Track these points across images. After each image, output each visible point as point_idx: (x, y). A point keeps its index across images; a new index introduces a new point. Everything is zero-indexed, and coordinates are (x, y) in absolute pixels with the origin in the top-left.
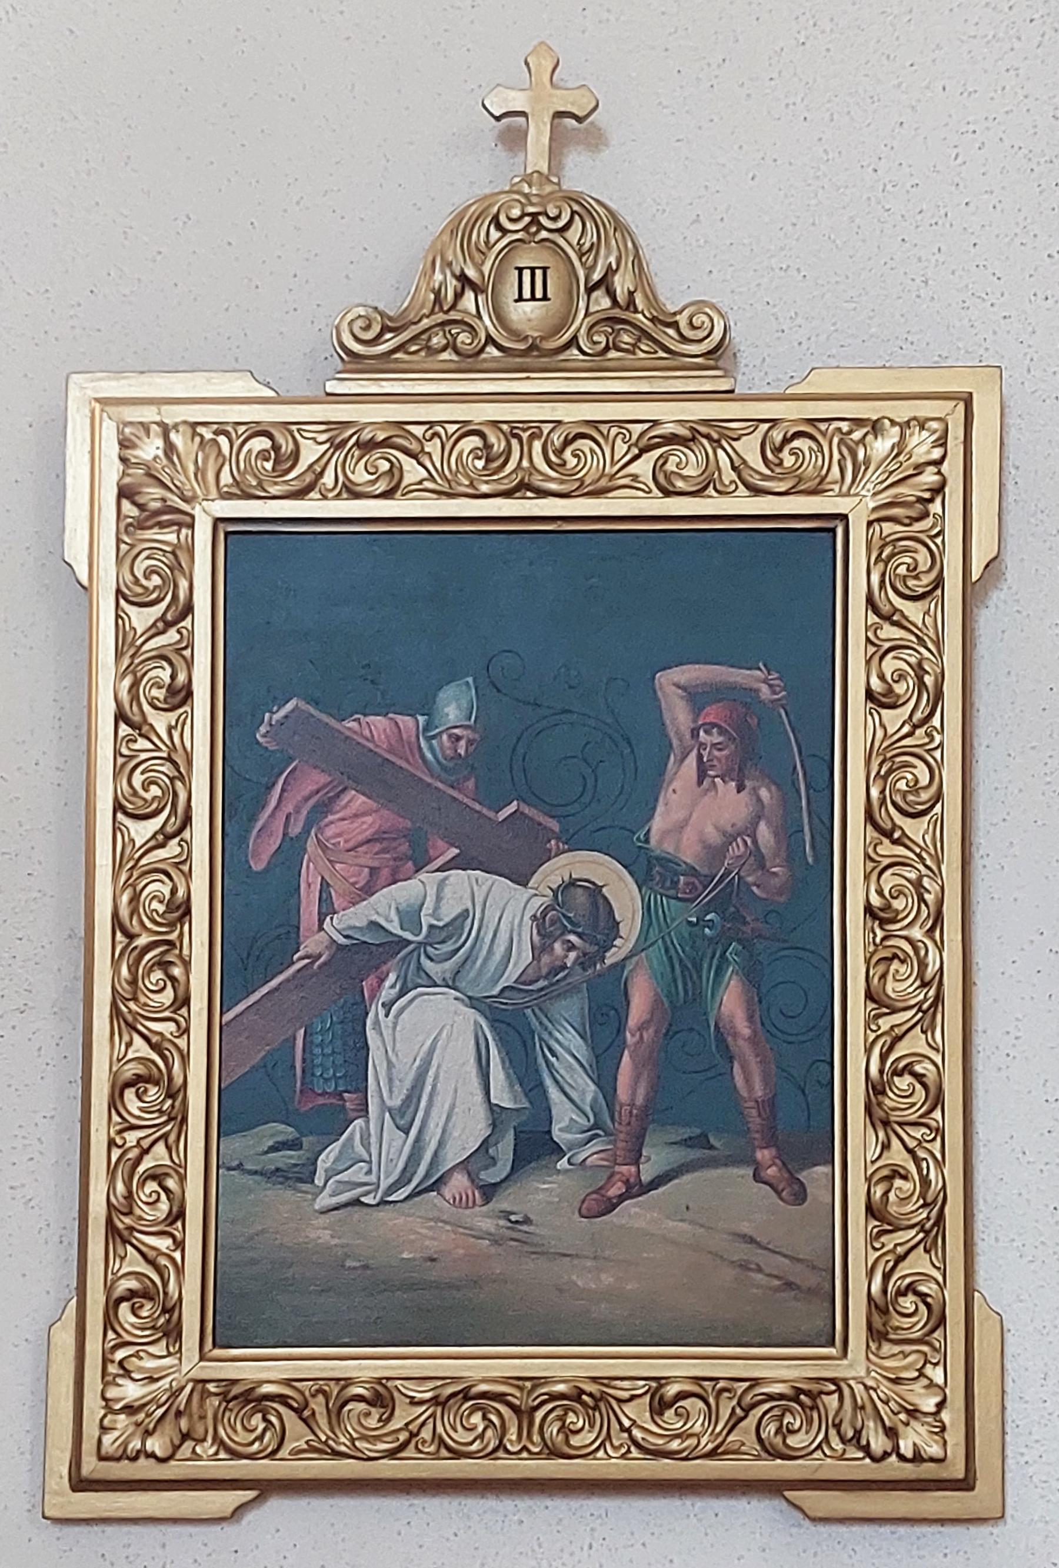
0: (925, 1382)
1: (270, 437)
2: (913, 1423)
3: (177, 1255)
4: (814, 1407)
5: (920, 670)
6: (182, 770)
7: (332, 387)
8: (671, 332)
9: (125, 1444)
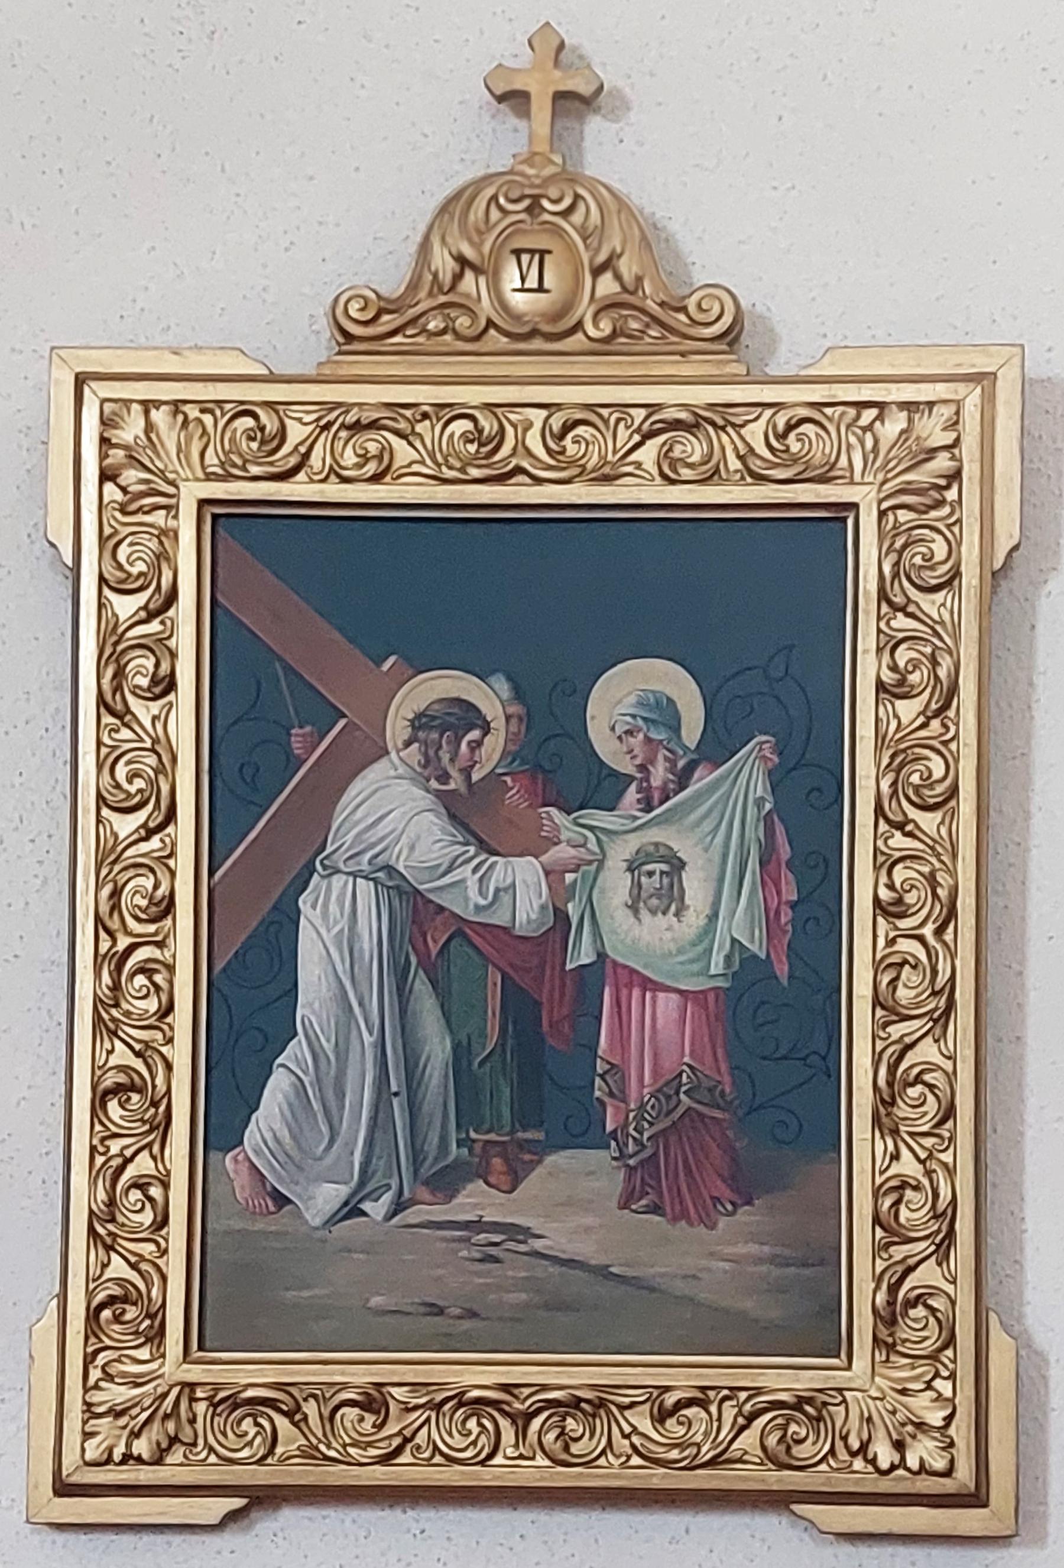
0: (934, 1395)
1: (255, 416)
2: (920, 1436)
3: (160, 1262)
4: (819, 1419)
5: (932, 880)
6: (165, 760)
8: (682, 317)
9: (110, 1450)
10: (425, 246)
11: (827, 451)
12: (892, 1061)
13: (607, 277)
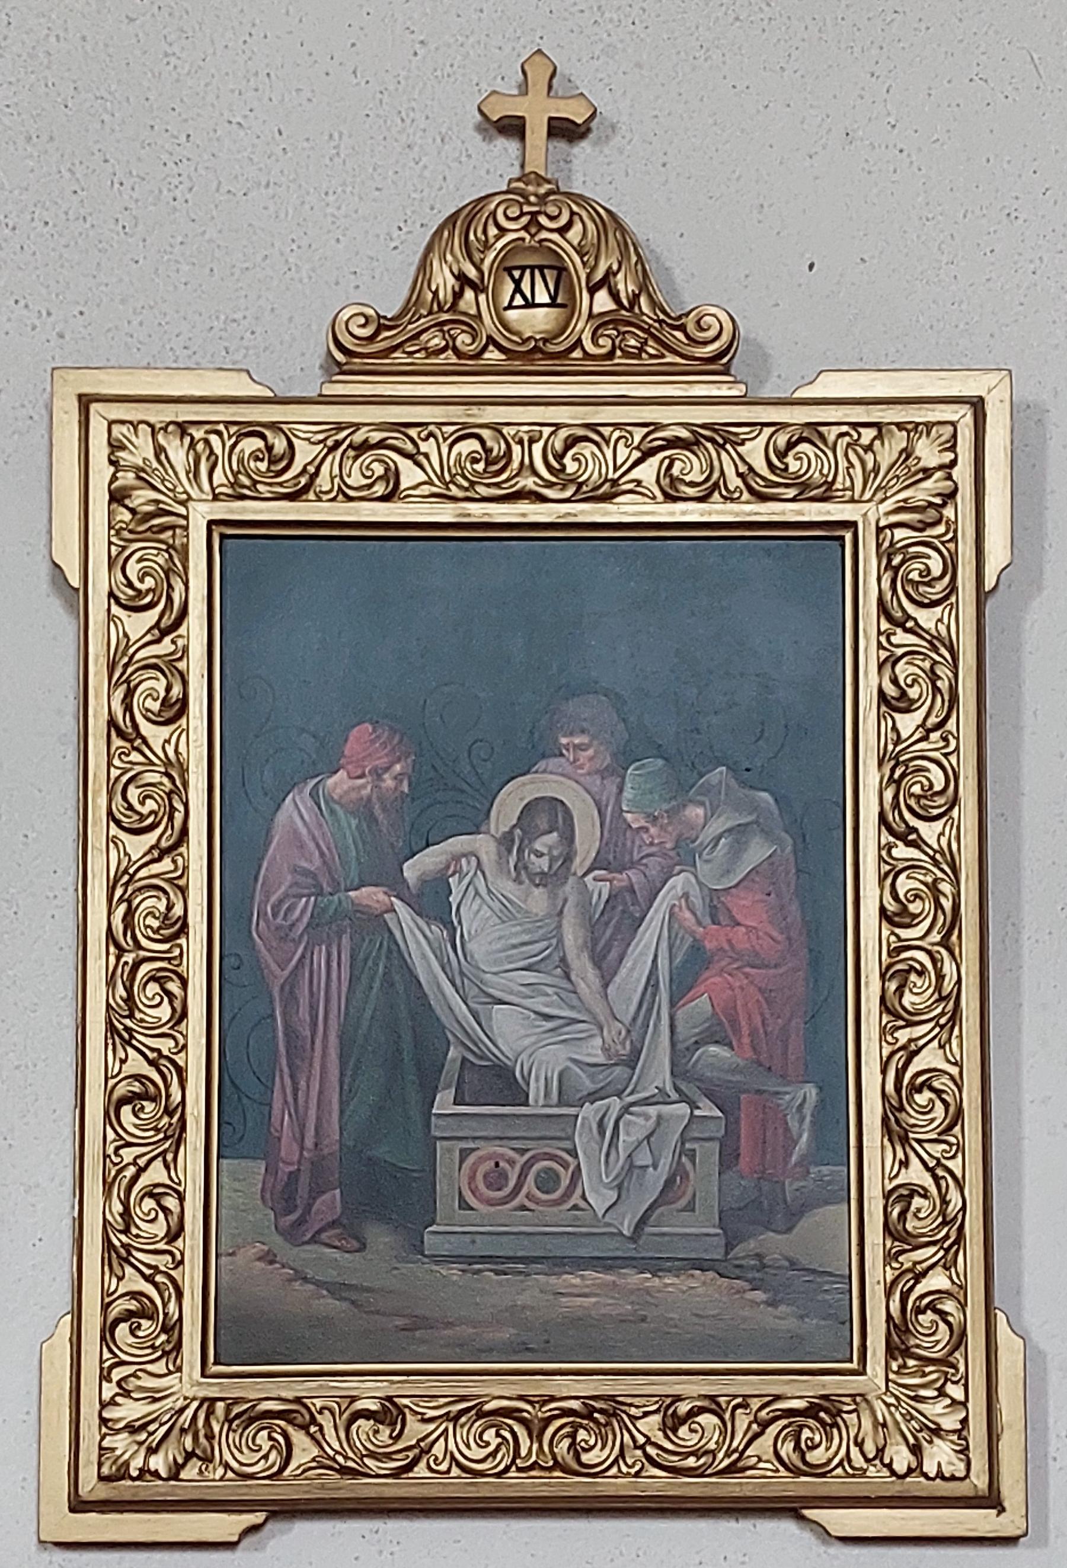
0: (948, 1401)
1: (263, 437)
2: (936, 1440)
5: (933, 677)
6: (178, 783)
7: (330, 390)
8: (679, 335)
10: (424, 265)
11: (825, 471)
12: (900, 1066)
13: (602, 296)
